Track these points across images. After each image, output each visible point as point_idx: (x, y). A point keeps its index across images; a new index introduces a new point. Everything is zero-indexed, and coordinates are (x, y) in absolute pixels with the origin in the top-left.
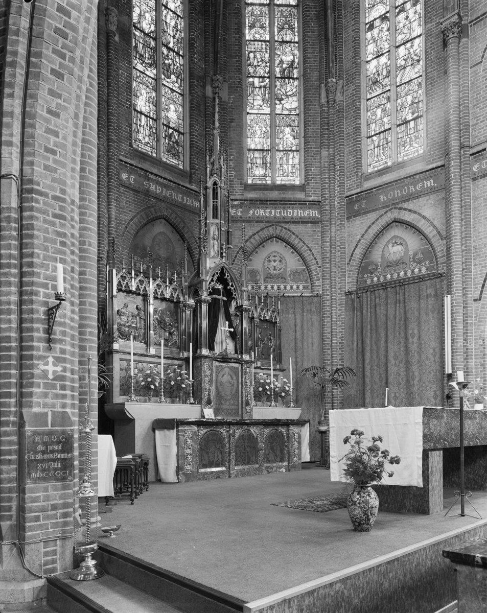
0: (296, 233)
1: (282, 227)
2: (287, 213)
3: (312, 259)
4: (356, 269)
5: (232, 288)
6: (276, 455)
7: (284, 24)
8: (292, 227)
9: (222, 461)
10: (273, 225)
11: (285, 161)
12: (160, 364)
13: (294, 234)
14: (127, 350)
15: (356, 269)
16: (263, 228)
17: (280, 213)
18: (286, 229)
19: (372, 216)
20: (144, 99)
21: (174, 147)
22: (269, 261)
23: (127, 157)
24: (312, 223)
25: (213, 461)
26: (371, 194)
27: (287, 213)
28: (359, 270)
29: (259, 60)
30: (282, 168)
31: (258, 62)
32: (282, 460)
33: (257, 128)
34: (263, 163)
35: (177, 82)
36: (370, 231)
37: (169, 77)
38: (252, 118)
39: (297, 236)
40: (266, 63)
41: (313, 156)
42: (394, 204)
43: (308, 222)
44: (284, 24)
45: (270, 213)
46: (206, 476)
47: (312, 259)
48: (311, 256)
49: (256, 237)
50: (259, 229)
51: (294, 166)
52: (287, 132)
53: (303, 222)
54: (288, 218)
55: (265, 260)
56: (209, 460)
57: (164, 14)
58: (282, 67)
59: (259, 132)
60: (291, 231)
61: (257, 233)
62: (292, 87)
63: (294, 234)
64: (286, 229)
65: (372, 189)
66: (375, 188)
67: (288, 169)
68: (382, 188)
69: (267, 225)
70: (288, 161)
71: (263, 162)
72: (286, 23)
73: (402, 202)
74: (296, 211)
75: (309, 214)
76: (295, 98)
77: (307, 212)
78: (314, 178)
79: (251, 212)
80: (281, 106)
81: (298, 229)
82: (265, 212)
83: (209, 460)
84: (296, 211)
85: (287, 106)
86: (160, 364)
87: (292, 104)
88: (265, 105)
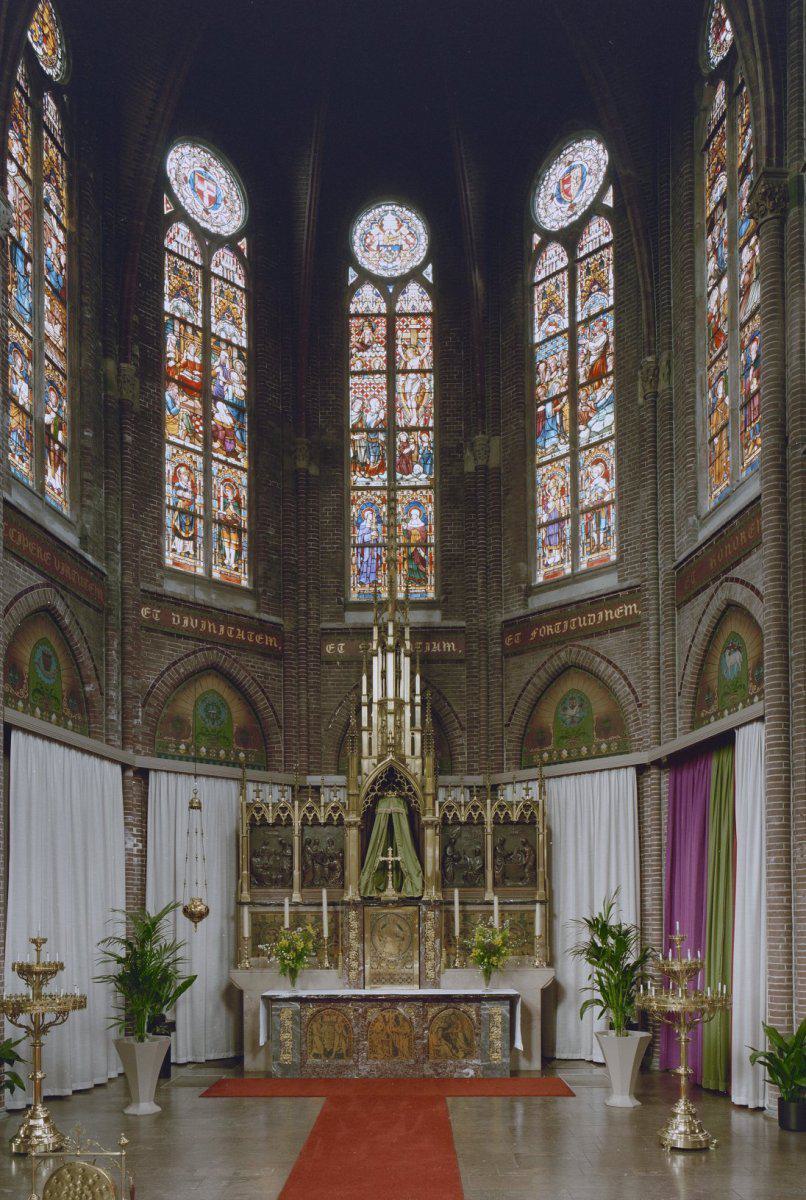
0: (601, 652)
5: (410, 794)
6: (455, 1047)
7: (592, 286)
8: (594, 642)
11: (594, 526)
17: (577, 622)
19: (703, 597)
21: (419, 570)
22: (565, 709)
23: (332, 621)
24: (627, 627)
29: (553, 369)
30: (588, 540)
35: (424, 472)
37: (409, 471)
38: (545, 470)
40: (563, 369)
43: (621, 628)
44: (592, 286)
45: (562, 627)
46: (317, 1070)
49: (542, 673)
51: (607, 530)
52: (595, 475)
53: (613, 630)
56: (325, 1050)
57: (401, 383)
59: (553, 491)
62: (604, 392)
63: (598, 654)
65: (617, 592)
66: (605, 595)
67: (599, 537)
68: (692, 561)
70: (598, 524)
71: (560, 539)
72: (595, 282)
75: (623, 613)
78: (630, 545)
80: (587, 431)
81: (609, 644)
82: (553, 628)
84: (601, 613)
85: (597, 427)
87: (604, 421)
88: (562, 441)
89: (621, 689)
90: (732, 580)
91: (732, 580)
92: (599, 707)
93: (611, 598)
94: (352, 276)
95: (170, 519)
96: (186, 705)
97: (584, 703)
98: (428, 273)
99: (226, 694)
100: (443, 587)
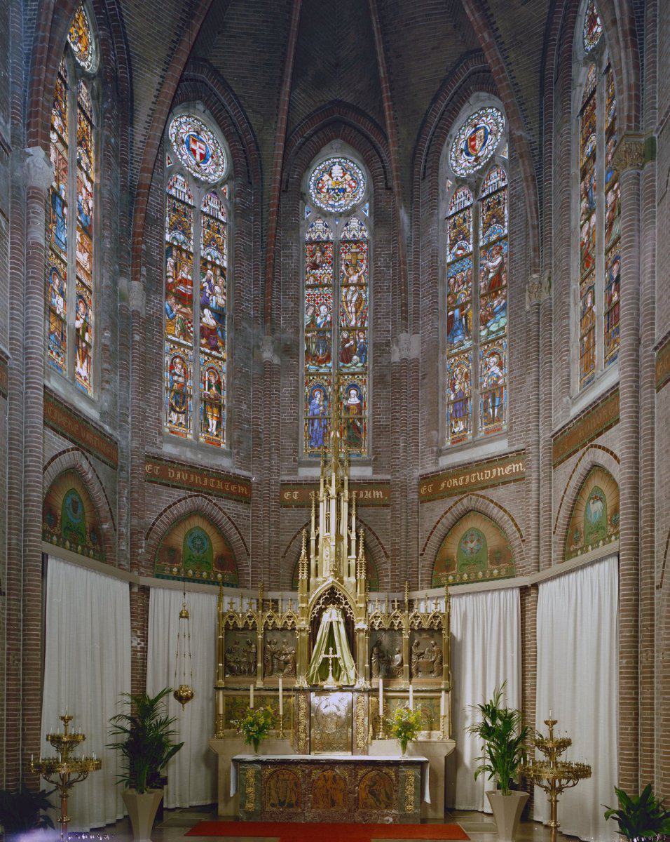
1: (478, 495)
4: (561, 540)
5: (347, 607)
7: (491, 219)
8: (489, 493)
12: (408, 698)
13: (492, 501)
14: (275, 687)
17: (476, 477)
18: (481, 496)
22: (466, 542)
24: (515, 481)
25: (284, 801)
26: (506, 460)
27: (484, 476)
28: (565, 540)
36: (433, 537)
41: (518, 388)
42: (471, 491)
43: (510, 482)
44: (491, 219)
50: (453, 503)
54: (485, 481)
56: (280, 800)
61: (449, 509)
64: (481, 496)
68: (565, 431)
69: (461, 496)
73: (483, 488)
74: (494, 470)
76: (503, 314)
77: (508, 468)
79: (443, 485)
81: (499, 493)
83: (280, 800)
86: (408, 698)
89: (510, 528)
92: (493, 541)
93: (503, 459)
96: (179, 539)
97: (481, 538)
99: (208, 529)
100: (376, 451)
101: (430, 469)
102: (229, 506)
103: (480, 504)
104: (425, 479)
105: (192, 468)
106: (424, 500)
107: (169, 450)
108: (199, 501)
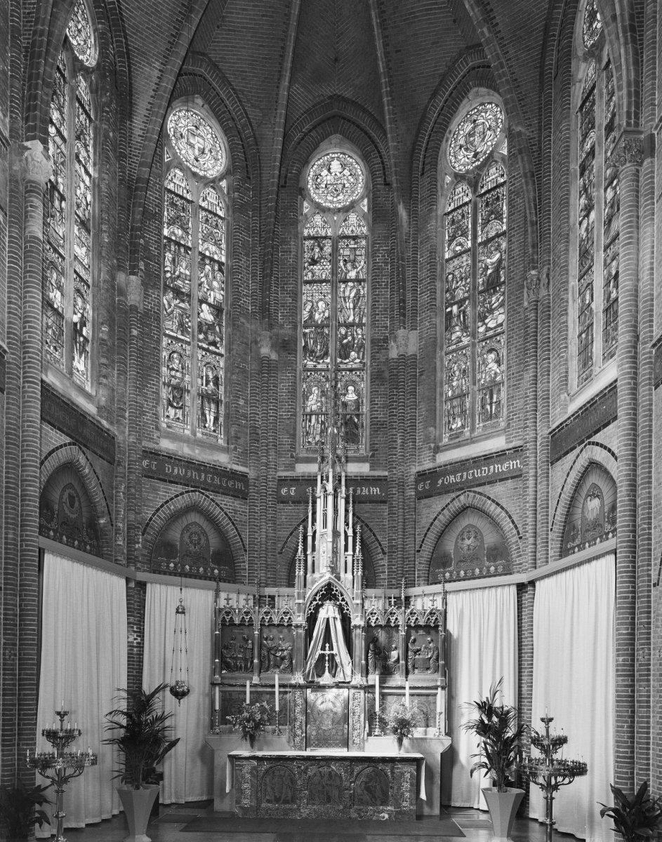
1: (475, 492)
2: (481, 473)
3: (512, 529)
8: (486, 489)
9: (292, 797)
10: (465, 492)
13: (489, 498)
14: (271, 683)
15: (558, 537)
16: (454, 499)
17: (473, 474)
20: (315, 398)
22: (463, 539)
24: (512, 478)
31: (457, 282)
32: (385, 803)
33: (455, 368)
34: (462, 412)
39: (493, 501)
43: (507, 479)
47: (512, 529)
48: (511, 524)
50: (448, 501)
53: (501, 480)
54: (482, 478)
55: (457, 538)
56: (275, 796)
57: (342, 290)
58: (485, 275)
60: (485, 496)
64: (480, 494)
68: (563, 428)
76: (501, 310)
79: (440, 482)
80: (484, 326)
81: (497, 490)
82: (455, 478)
83: (275, 796)
89: (507, 525)
90: (593, 443)
91: (593, 443)
92: (490, 539)
93: (501, 455)
94: (306, 208)
95: (165, 393)
96: (175, 534)
97: (478, 535)
98: (365, 206)
100: (373, 449)
101: (427, 465)
102: (227, 502)
103: (478, 501)
104: (422, 476)
105: (189, 464)
106: (422, 496)
107: (166, 445)
108: (196, 496)
